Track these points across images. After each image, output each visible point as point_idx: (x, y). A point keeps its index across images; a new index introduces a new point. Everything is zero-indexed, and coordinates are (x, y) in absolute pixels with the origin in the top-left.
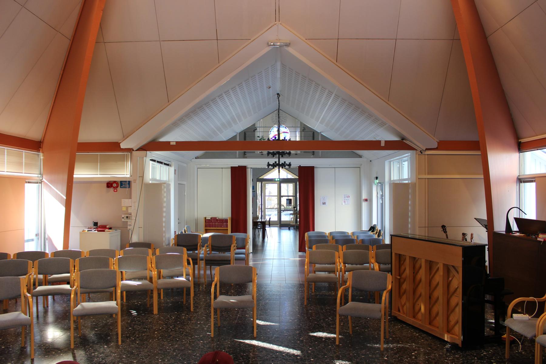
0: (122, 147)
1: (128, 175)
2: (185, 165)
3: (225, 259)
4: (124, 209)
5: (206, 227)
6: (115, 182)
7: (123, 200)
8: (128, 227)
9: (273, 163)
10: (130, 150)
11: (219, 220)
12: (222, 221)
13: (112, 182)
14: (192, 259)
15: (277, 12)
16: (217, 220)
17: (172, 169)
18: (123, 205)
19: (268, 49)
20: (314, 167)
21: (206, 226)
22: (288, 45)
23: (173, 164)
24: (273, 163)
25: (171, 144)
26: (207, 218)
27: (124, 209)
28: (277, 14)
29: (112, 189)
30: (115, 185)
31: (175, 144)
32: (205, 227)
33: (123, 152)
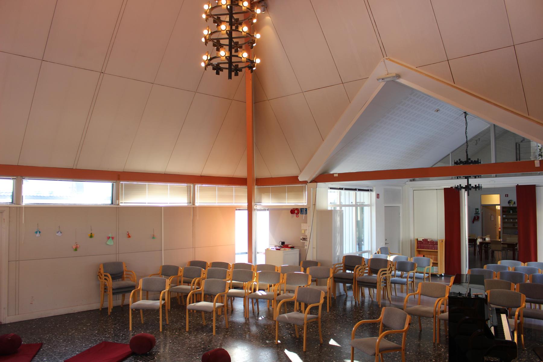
0: (300, 180)
1: (305, 203)
2: (401, 188)
3: (372, 282)
4: (303, 232)
5: (418, 249)
6: (297, 209)
7: (302, 224)
8: (305, 247)
9: (466, 186)
10: (305, 182)
11: (430, 242)
12: (433, 243)
13: (295, 209)
14: (110, 274)
15: (383, 48)
16: (428, 242)
17: (374, 194)
18: (302, 228)
19: (382, 84)
20: (535, 185)
21: (418, 248)
22: (398, 76)
23: (374, 189)
24: (466, 186)
25: (335, 175)
26: (418, 240)
27: (303, 232)
28: (383, 51)
29: (295, 215)
30: (296, 212)
31: (337, 175)
32: (417, 248)
33: (302, 184)
